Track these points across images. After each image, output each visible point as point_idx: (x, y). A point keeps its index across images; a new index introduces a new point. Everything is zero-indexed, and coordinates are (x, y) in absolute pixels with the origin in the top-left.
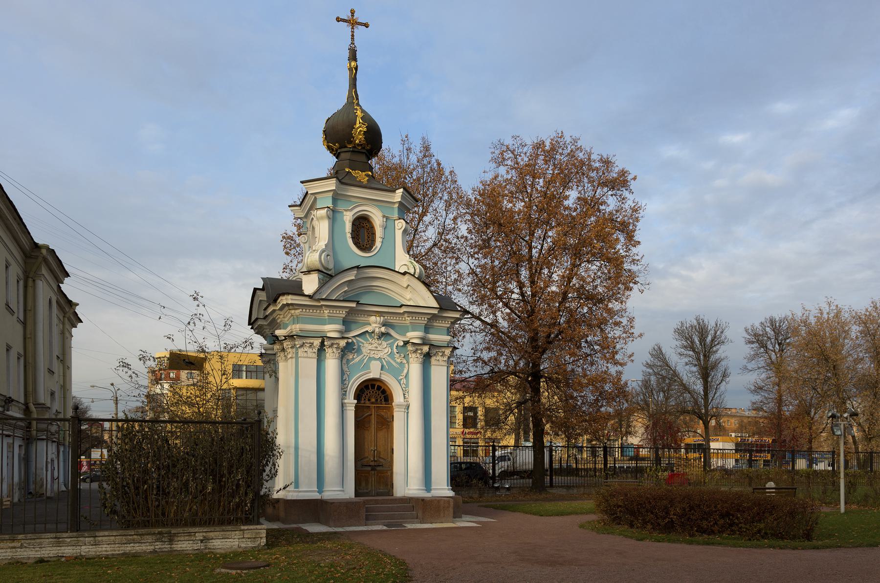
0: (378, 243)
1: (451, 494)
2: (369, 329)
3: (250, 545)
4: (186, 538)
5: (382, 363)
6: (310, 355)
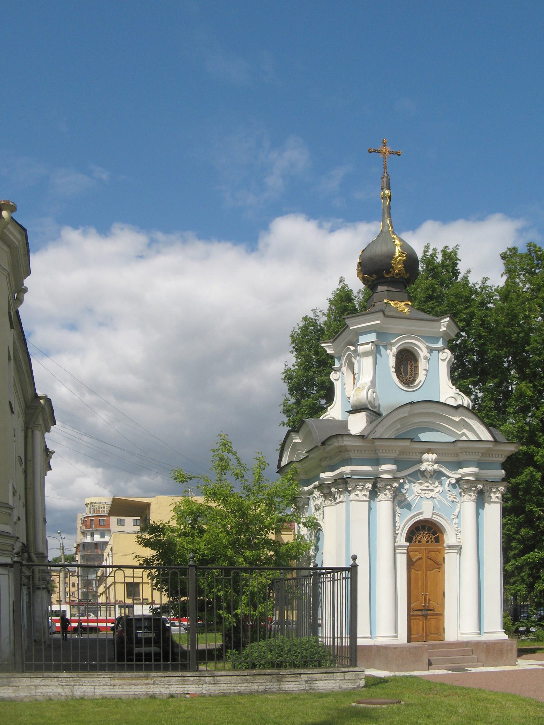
0: (421, 377)
1: (506, 637)
3: (351, 686)
4: (293, 679)
6: (361, 497)
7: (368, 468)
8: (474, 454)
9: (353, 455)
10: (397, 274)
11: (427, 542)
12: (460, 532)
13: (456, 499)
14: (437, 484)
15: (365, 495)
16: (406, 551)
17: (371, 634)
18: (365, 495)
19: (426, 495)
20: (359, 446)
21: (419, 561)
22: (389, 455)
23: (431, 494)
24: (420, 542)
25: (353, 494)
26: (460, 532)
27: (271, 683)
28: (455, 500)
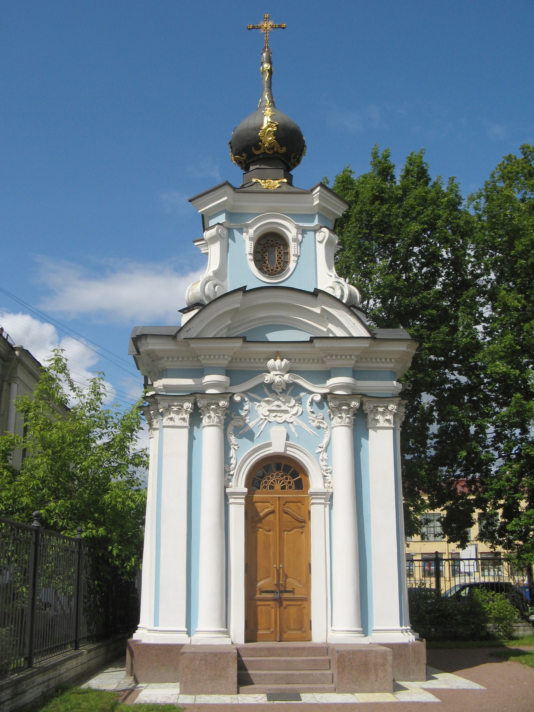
0: (292, 265)
5: (289, 429)
6: (178, 423)
7: (189, 382)
8: (344, 357)
9: (168, 364)
10: (269, 149)
11: (283, 488)
12: (331, 473)
13: (323, 423)
14: (293, 402)
15: (183, 419)
16: (243, 501)
18: (183, 419)
19: (278, 419)
20: (169, 350)
21: (271, 516)
22: (215, 362)
23: (286, 417)
24: (272, 487)
25: (165, 419)
26: (331, 473)
28: (321, 425)
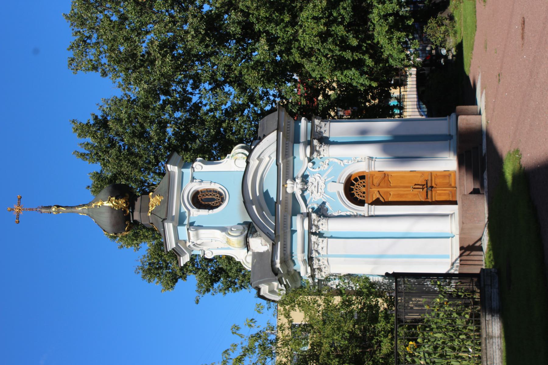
0: (216, 187)
2: (298, 194)
5: (329, 181)
11: (364, 186)
17: (449, 237)
19: (323, 188)
24: (364, 193)
27: (494, 344)
28: (327, 163)
